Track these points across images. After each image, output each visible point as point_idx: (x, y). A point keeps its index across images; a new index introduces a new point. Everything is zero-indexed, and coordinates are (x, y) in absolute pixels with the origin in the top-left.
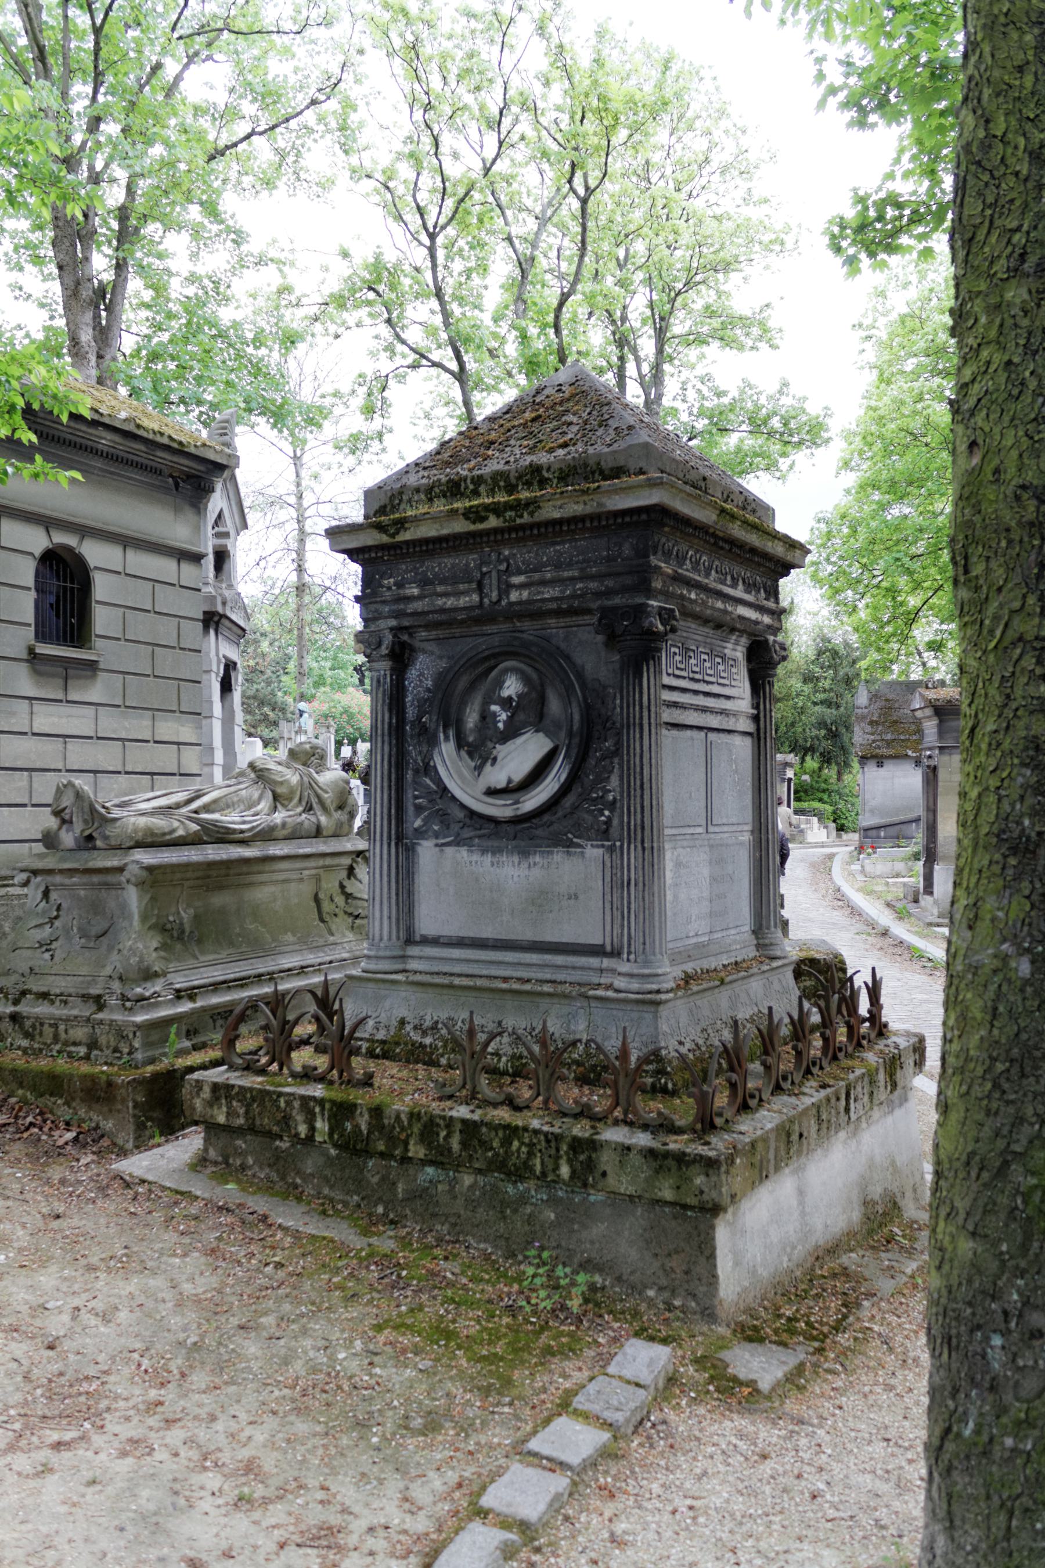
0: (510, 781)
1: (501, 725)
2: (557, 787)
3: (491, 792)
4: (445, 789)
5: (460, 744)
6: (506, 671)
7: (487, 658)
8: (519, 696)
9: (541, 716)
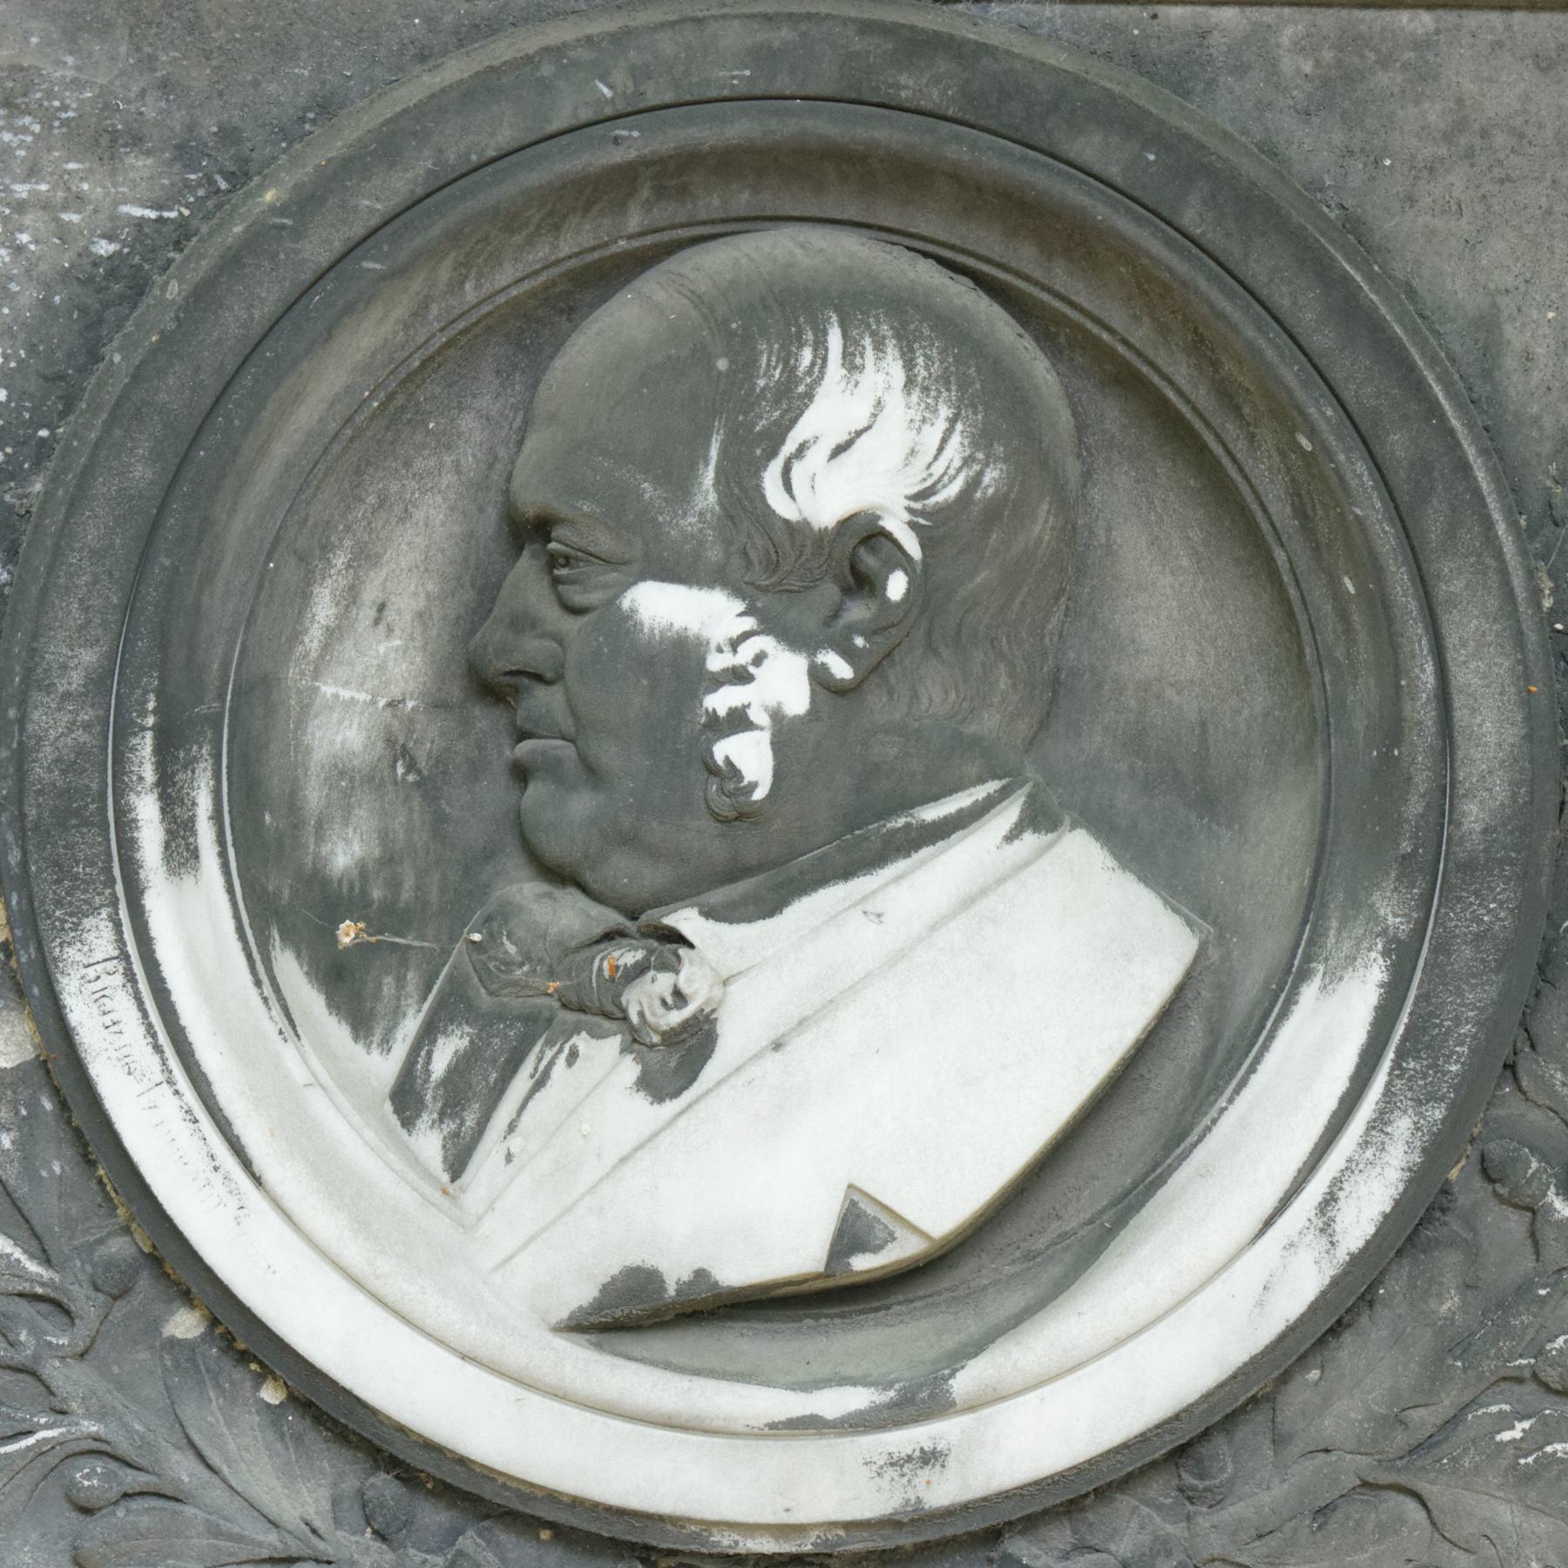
0: (854, 1230)
1: (751, 757)
2: (1298, 1280)
3: (640, 1313)
4: (175, 1266)
5: (284, 907)
6: (794, 310)
7: (609, 188)
8: (937, 525)
9: (1056, 695)
